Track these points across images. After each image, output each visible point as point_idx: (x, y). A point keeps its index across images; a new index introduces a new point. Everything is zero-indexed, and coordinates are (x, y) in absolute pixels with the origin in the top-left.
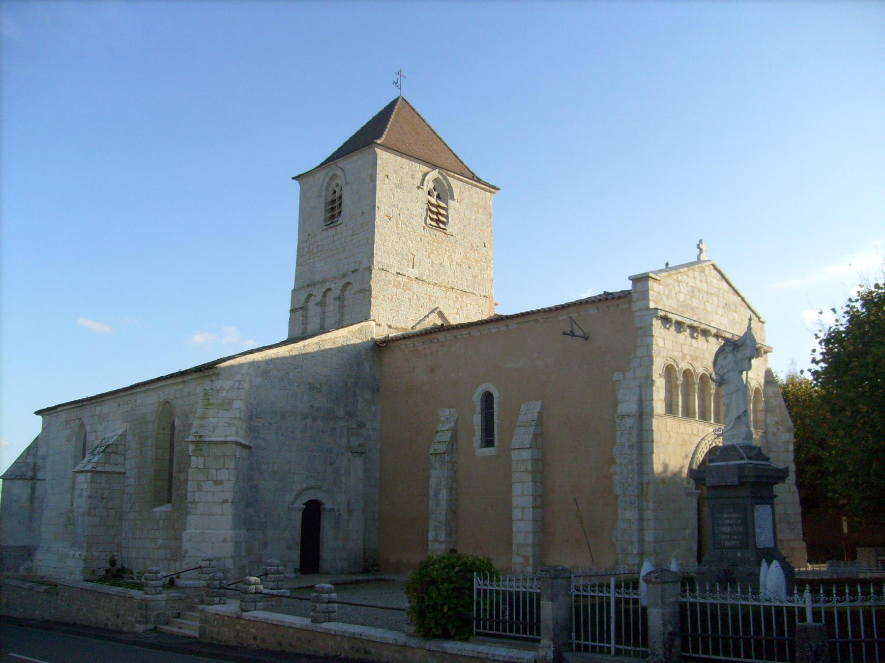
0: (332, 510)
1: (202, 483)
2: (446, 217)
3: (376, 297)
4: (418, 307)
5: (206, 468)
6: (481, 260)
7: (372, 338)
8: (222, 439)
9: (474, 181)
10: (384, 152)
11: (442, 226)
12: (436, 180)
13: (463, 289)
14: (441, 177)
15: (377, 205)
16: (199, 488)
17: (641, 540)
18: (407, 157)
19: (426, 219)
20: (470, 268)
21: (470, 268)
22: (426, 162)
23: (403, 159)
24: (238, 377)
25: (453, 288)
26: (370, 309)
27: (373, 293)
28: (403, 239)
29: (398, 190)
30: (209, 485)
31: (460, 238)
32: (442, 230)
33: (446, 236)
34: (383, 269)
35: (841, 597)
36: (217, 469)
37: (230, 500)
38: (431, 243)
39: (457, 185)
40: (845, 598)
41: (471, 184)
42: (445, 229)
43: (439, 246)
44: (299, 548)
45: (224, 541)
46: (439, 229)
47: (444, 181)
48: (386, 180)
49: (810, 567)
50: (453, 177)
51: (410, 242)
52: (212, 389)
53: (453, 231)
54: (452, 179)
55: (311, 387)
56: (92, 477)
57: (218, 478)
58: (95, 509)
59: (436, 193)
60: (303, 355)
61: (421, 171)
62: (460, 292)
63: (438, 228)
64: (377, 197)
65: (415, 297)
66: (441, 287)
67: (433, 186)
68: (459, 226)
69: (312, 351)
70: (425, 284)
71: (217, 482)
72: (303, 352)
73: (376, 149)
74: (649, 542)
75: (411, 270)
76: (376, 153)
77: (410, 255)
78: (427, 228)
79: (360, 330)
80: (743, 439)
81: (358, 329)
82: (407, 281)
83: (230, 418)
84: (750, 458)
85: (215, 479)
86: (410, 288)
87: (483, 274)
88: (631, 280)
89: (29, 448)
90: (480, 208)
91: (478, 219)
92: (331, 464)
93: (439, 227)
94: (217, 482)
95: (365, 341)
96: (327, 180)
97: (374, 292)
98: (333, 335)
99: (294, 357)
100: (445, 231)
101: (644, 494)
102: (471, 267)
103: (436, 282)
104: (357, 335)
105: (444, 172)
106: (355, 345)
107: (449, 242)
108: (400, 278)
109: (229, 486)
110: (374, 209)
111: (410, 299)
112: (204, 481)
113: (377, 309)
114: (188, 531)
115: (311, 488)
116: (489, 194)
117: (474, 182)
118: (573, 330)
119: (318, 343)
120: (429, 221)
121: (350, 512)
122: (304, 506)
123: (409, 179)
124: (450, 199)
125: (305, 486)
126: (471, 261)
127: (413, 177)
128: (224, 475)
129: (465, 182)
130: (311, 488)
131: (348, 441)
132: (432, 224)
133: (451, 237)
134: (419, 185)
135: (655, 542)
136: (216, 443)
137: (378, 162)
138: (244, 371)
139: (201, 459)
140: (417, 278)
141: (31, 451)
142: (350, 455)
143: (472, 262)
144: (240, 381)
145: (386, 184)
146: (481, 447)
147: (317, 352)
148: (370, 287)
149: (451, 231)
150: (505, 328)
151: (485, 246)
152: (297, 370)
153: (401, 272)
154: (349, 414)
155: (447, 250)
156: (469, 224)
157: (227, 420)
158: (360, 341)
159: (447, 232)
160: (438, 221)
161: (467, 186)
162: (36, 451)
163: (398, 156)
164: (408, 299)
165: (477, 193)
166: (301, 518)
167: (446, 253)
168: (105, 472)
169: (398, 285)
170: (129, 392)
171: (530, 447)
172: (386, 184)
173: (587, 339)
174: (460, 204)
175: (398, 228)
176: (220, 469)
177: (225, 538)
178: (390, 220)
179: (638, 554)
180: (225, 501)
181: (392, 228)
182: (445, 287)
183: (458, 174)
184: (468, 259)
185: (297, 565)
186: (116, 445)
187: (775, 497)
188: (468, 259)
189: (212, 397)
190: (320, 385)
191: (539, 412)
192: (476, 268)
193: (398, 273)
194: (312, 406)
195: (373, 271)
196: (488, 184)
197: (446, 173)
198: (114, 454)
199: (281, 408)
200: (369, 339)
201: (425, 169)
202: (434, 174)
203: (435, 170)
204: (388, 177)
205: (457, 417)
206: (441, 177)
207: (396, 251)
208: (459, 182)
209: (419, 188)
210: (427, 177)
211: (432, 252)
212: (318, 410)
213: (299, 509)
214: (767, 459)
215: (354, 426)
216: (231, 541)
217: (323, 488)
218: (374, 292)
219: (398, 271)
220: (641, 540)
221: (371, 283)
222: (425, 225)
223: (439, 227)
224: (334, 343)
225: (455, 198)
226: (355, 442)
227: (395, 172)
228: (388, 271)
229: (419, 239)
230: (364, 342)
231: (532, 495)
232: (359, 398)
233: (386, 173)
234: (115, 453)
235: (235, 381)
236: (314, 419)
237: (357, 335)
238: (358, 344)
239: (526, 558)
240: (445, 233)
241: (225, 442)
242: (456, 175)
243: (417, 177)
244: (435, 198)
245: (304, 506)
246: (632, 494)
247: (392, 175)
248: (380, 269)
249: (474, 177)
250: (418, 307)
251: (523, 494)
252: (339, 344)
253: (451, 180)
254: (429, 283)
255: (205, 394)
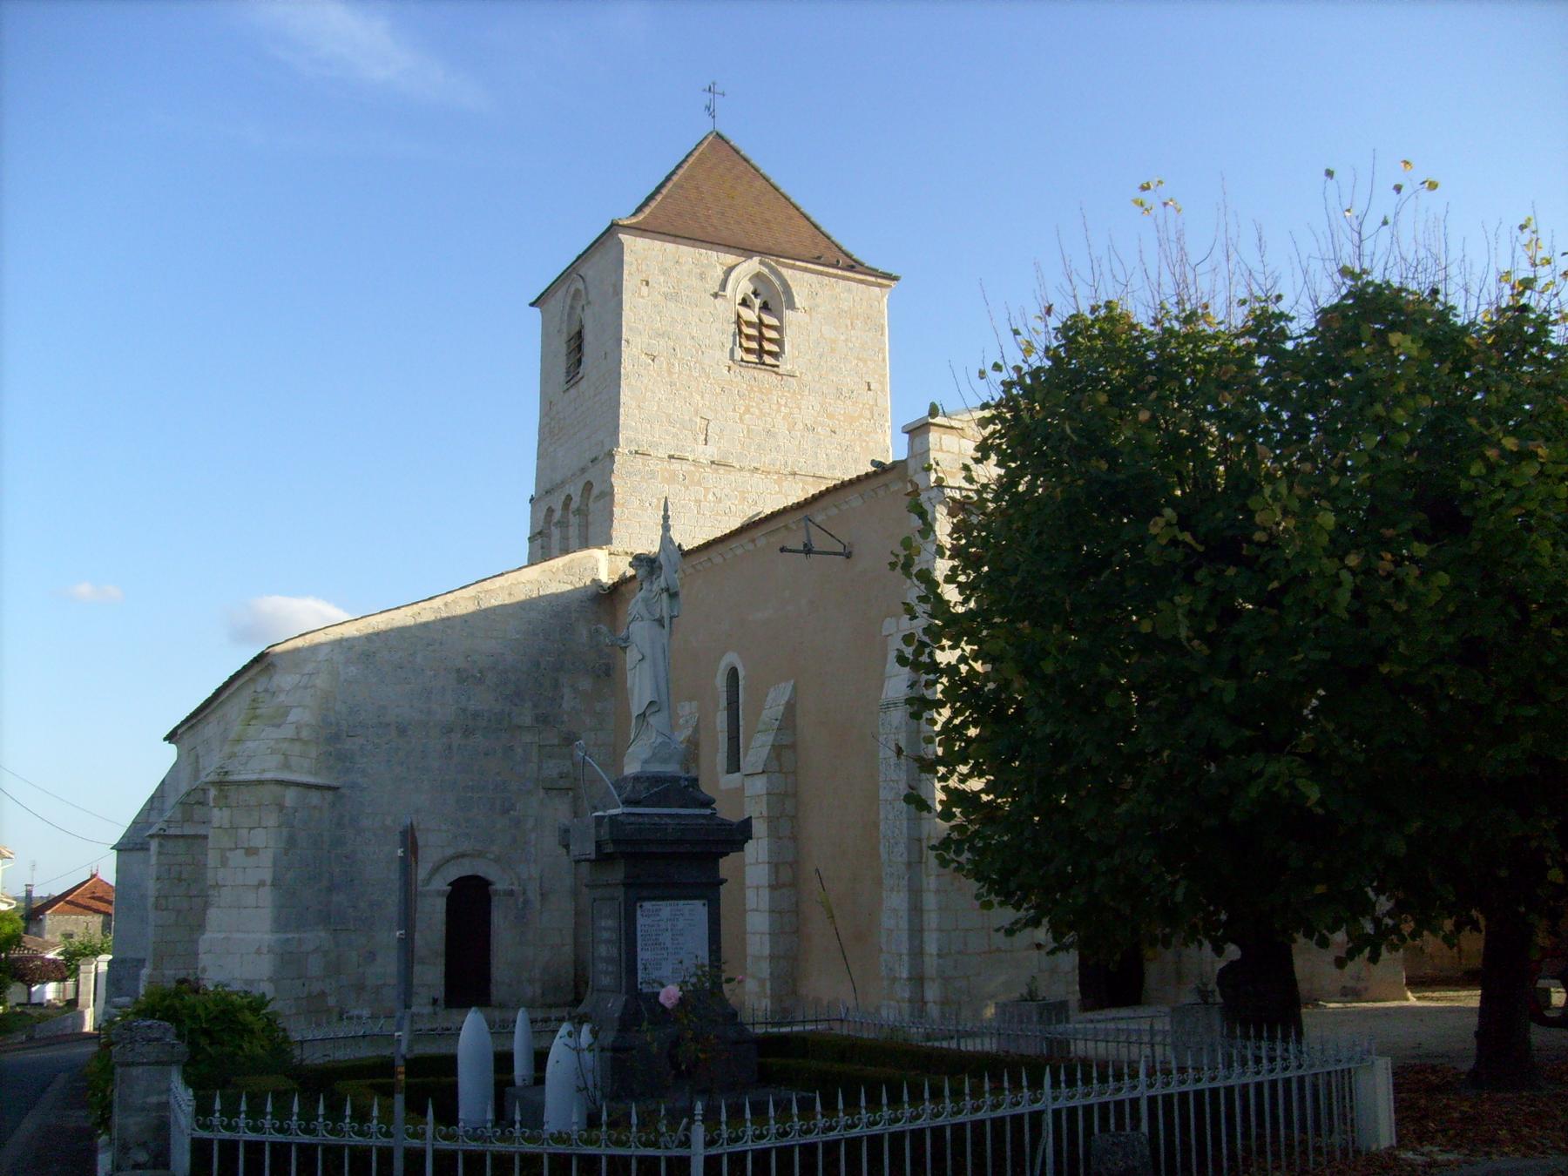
0: (511, 893)
1: (228, 854)
2: (779, 343)
3: (623, 504)
4: (718, 514)
5: (234, 828)
6: (861, 416)
7: (594, 580)
8: (254, 777)
9: (840, 268)
10: (638, 239)
11: (768, 359)
12: (757, 277)
13: (819, 474)
14: (765, 271)
15: (624, 337)
16: (224, 862)
17: (917, 953)
18: (685, 240)
19: (732, 351)
20: (835, 432)
21: (835, 432)
22: (729, 246)
23: (680, 246)
24: (309, 667)
25: (795, 474)
26: (611, 526)
27: (618, 497)
28: (683, 393)
29: (671, 305)
30: (237, 858)
31: (810, 378)
32: (768, 368)
33: (780, 378)
34: (636, 452)
35: (255, 1120)
36: (251, 829)
37: (269, 882)
38: (744, 394)
39: (802, 282)
40: (236, 1122)
41: (835, 276)
42: (777, 366)
43: (765, 398)
44: (443, 961)
45: (258, 952)
46: (764, 367)
47: (773, 278)
48: (645, 290)
49: (1412, 1000)
50: (793, 267)
51: (699, 398)
52: (266, 691)
53: (796, 367)
54: (790, 271)
55: (462, 676)
56: (161, 845)
57: (252, 844)
58: (166, 897)
59: (757, 302)
60: (443, 620)
61: (721, 264)
62: (811, 479)
63: (759, 366)
64: (624, 323)
65: (710, 497)
66: (769, 473)
67: (752, 288)
68: (808, 357)
69: (465, 612)
70: (730, 471)
71: (251, 851)
72: (444, 615)
73: (620, 235)
74: (931, 955)
75: (701, 447)
76: (621, 244)
77: (698, 420)
78: (735, 368)
79: (568, 568)
80: (646, 762)
81: (563, 566)
82: (693, 468)
83: (277, 740)
84: (627, 803)
85: (246, 846)
86: (699, 480)
87: (865, 441)
88: (907, 433)
89: (153, 798)
90: (857, 319)
91: (854, 339)
92: (505, 811)
93: (764, 364)
94: (251, 851)
95: (577, 586)
96: (569, 301)
97: (620, 496)
98: (507, 581)
99: (426, 625)
100: (775, 369)
101: (924, 860)
102: (837, 430)
103: (757, 465)
104: (562, 576)
105: (772, 260)
106: (557, 596)
107: (786, 389)
108: (676, 465)
109: (266, 858)
110: (620, 345)
111: (698, 502)
112: (230, 849)
113: (627, 527)
114: (208, 936)
115: (463, 855)
116: (877, 290)
117: (840, 272)
118: (809, 541)
119: (477, 598)
120: (739, 354)
121: (543, 896)
122: (450, 888)
123: (695, 282)
124: (787, 308)
125: (450, 852)
126: (838, 420)
127: (702, 276)
128: (260, 838)
129: (821, 273)
130: (463, 855)
131: (540, 768)
132: (745, 359)
133: (790, 379)
134: (716, 289)
135: (939, 956)
136: (248, 783)
137: (625, 258)
138: (321, 657)
139: (226, 813)
140: (713, 462)
141: (156, 804)
142: (542, 793)
143: (840, 421)
144: (310, 675)
145: (643, 297)
146: (728, 772)
147: (473, 614)
148: (612, 487)
149: (789, 367)
150: (750, 547)
151: (869, 389)
152: (430, 648)
153: (677, 454)
154: (543, 720)
155: (783, 403)
156: (833, 350)
157: (272, 743)
158: (570, 587)
159: (780, 371)
160: (761, 352)
161: (826, 280)
162: (163, 802)
163: (669, 242)
164: (696, 501)
165: (849, 291)
166: (444, 910)
167: (779, 411)
168: (183, 836)
169: (672, 478)
170: (215, 704)
171: (763, 772)
172: (643, 297)
173: (848, 556)
174: (811, 316)
175: (670, 373)
176: (254, 828)
177: (259, 949)
178: (653, 360)
179: (910, 979)
180: (262, 884)
181: (658, 375)
182: (777, 473)
183: (803, 261)
184: (831, 416)
185: (440, 992)
186: (203, 790)
187: (721, 884)
188: (831, 416)
189: (261, 705)
190: (481, 672)
191: (788, 702)
192: (850, 432)
193: (671, 457)
194: (464, 710)
195: (617, 458)
196: (877, 271)
197: (777, 262)
198: (200, 806)
199: (397, 716)
200: (588, 583)
201: (730, 259)
202: (753, 265)
203: (751, 258)
204: (647, 284)
205: (699, 718)
206: (765, 271)
207: (668, 416)
208: (807, 276)
209: (716, 295)
210: (733, 275)
211: (747, 411)
212: (476, 715)
213: (439, 893)
214: (708, 803)
215: (556, 741)
216: (269, 952)
217: (488, 855)
218: (620, 496)
219: (672, 453)
220: (917, 953)
221: (613, 480)
222: (731, 362)
223: (764, 364)
224: (510, 594)
225: (798, 305)
226: (552, 768)
227: (664, 272)
228: (649, 455)
229: (718, 390)
230: (576, 589)
231: (769, 863)
232: (567, 691)
233: (644, 276)
234: (200, 803)
235: (303, 675)
236: (468, 732)
237: (562, 576)
238: (562, 594)
239: (762, 982)
240: (777, 373)
241: (261, 782)
242: (798, 263)
243: (712, 276)
244: (757, 310)
245: (450, 888)
246: (900, 859)
247: (657, 279)
248: (631, 452)
249: (854, 266)
250: (718, 514)
251: (758, 863)
252: (520, 596)
253: (786, 273)
254: (741, 469)
255: (254, 700)
